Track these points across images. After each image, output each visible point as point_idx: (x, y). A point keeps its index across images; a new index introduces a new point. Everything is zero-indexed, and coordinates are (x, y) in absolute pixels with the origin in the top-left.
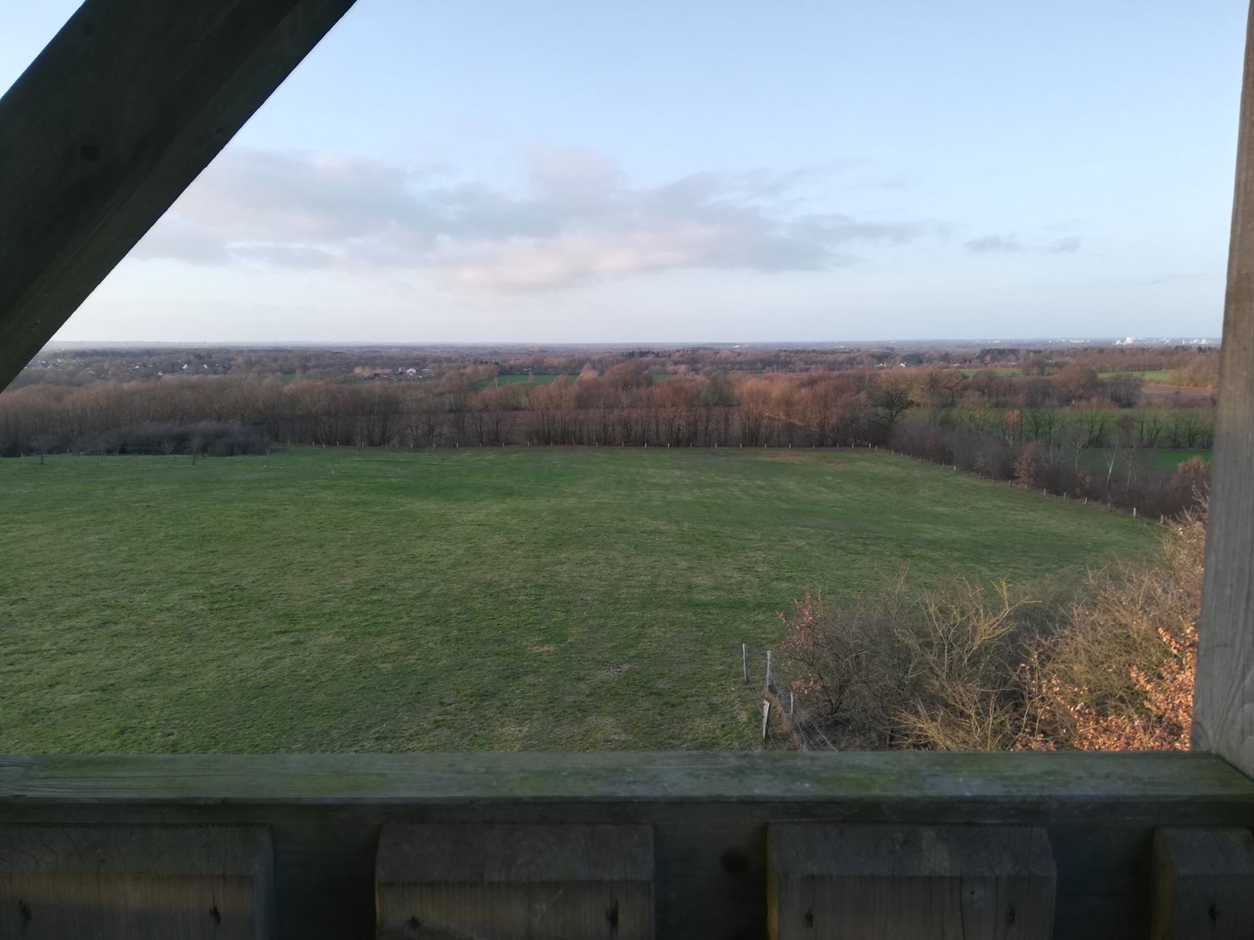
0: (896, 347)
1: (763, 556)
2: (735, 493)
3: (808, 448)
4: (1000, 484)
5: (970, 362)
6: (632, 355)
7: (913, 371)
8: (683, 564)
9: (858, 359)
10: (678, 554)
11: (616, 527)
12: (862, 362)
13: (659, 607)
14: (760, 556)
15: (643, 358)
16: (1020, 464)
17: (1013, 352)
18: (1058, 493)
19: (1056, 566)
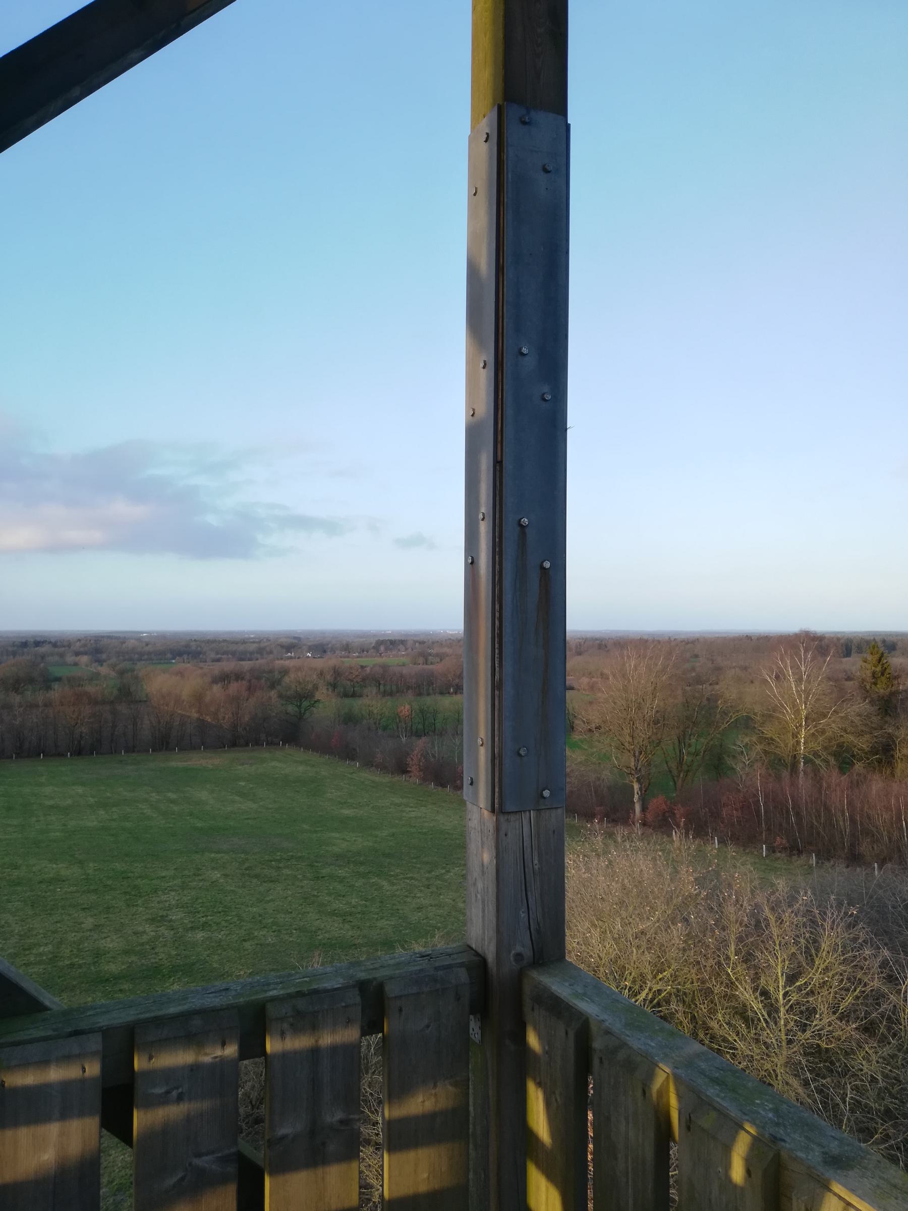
0: (302, 636)
1: (176, 898)
2: (145, 811)
3: (220, 750)
4: (396, 778)
5: (367, 652)
6: (25, 644)
7: (319, 663)
8: (89, 922)
9: (268, 649)
10: (84, 909)
11: (8, 878)
12: (271, 652)
13: (63, 991)
14: (174, 899)
15: (38, 648)
16: (412, 759)
17: (403, 642)
18: (443, 785)
19: (443, 871)
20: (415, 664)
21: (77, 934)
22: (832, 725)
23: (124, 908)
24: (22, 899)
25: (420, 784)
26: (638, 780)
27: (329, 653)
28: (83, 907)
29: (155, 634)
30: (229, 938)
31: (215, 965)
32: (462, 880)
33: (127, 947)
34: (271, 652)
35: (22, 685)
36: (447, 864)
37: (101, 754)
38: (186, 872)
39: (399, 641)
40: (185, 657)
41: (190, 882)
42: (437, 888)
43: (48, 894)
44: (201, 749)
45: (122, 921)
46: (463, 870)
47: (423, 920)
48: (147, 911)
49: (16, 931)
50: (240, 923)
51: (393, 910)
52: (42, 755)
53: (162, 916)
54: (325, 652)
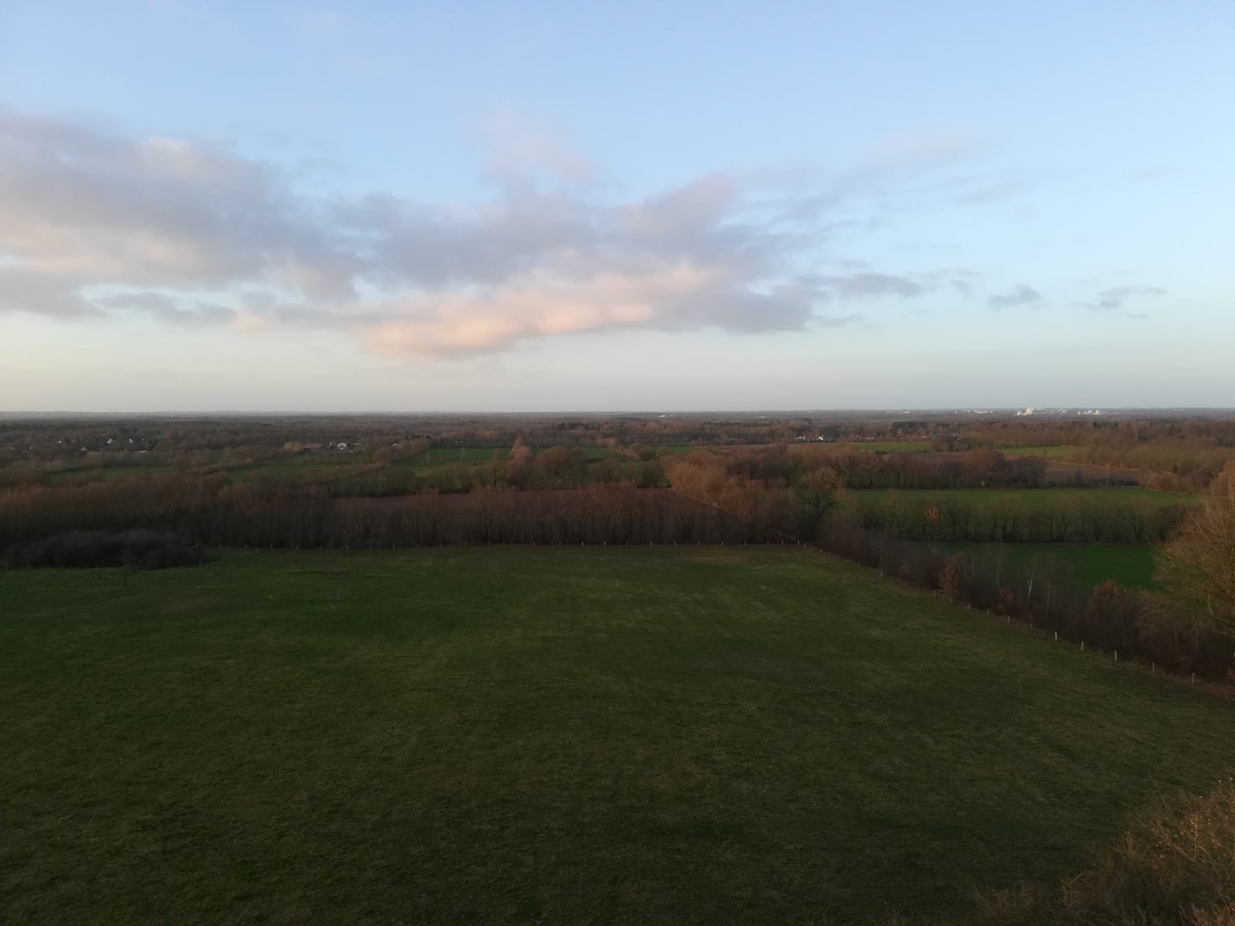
5: (884, 435)
6: (562, 427)
16: (944, 576)
17: (923, 424)
19: (994, 731)
27: (842, 437)
29: (672, 416)
34: (782, 435)
53: (705, 755)
54: (838, 435)
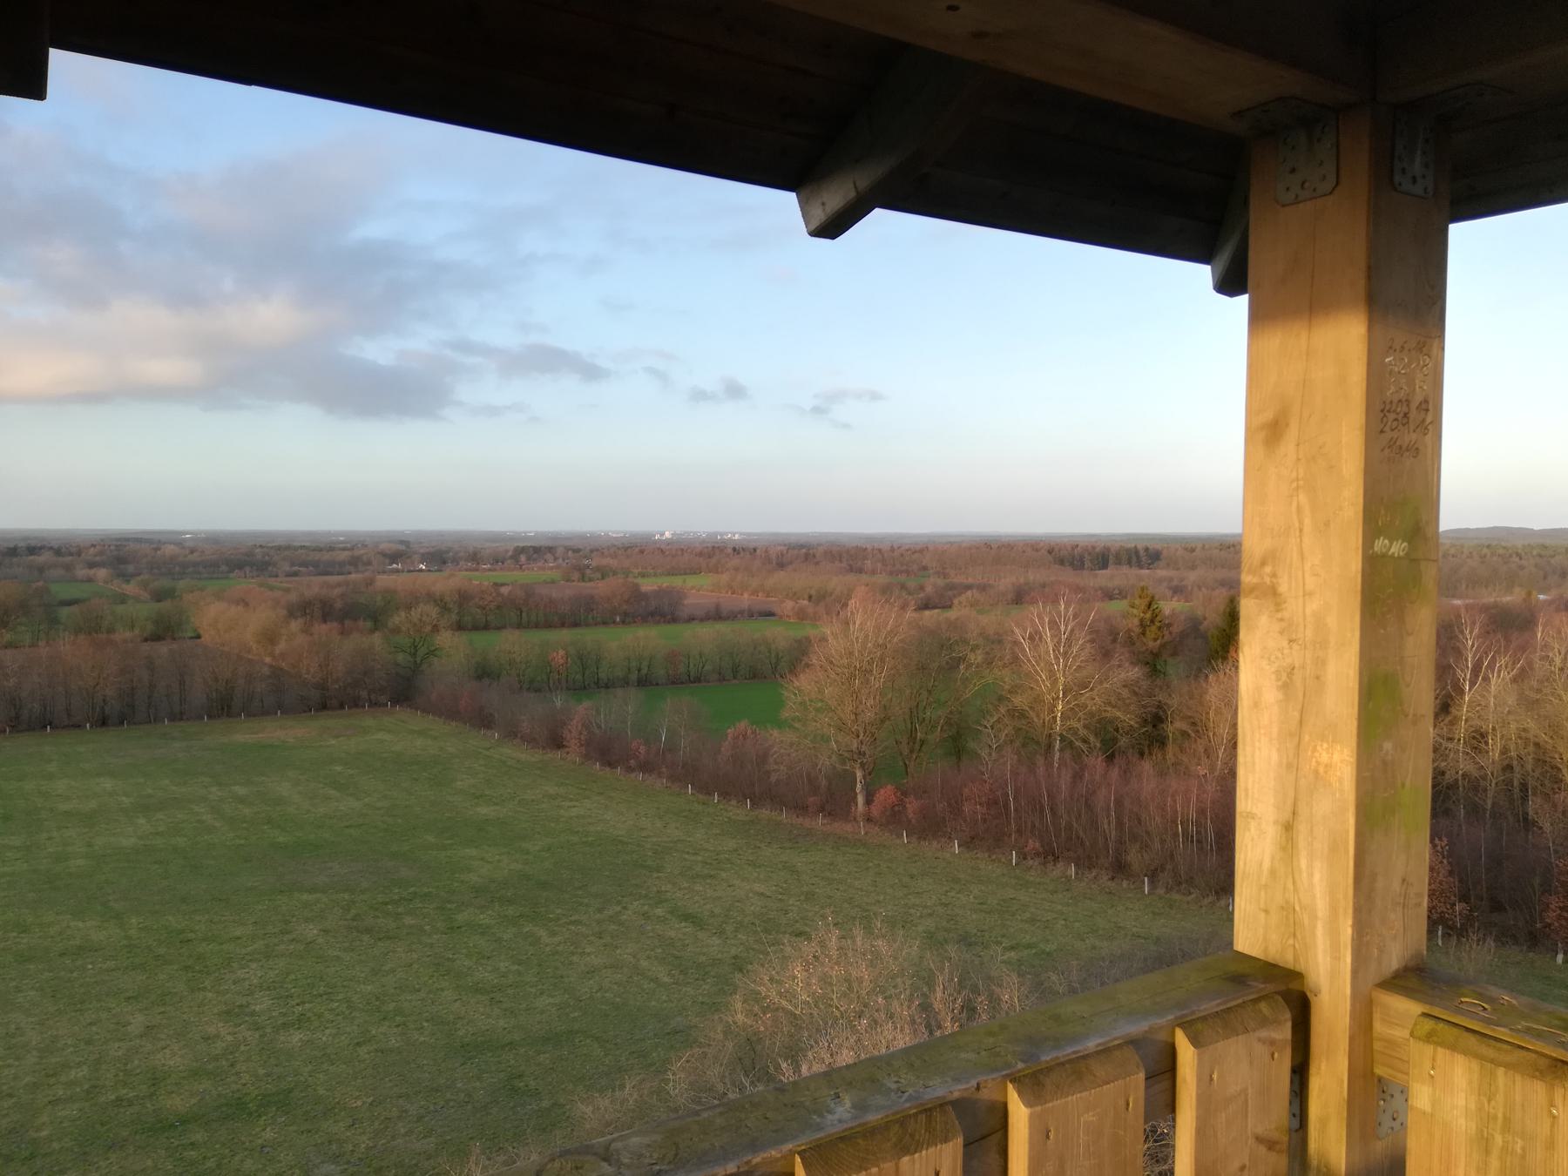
2: (204, 818)
5: (503, 563)
9: (365, 558)
16: (570, 732)
17: (551, 549)
19: (619, 908)
20: (567, 581)
21: (121, 1044)
22: (1093, 700)
23: (186, 993)
24: (37, 985)
25: (583, 763)
26: (863, 765)
28: (127, 994)
30: (337, 1041)
31: (321, 1091)
32: (643, 922)
33: (195, 1064)
34: (369, 563)
35: (13, 617)
36: (623, 897)
37: (135, 724)
38: (271, 927)
39: (546, 548)
40: (247, 569)
41: (276, 945)
42: (612, 937)
43: (75, 974)
44: (276, 714)
45: (185, 1016)
46: (644, 905)
47: (596, 992)
48: (219, 998)
49: (34, 1043)
50: (351, 1013)
51: (557, 978)
52: (48, 727)
53: (241, 1006)
54: (444, 562)
